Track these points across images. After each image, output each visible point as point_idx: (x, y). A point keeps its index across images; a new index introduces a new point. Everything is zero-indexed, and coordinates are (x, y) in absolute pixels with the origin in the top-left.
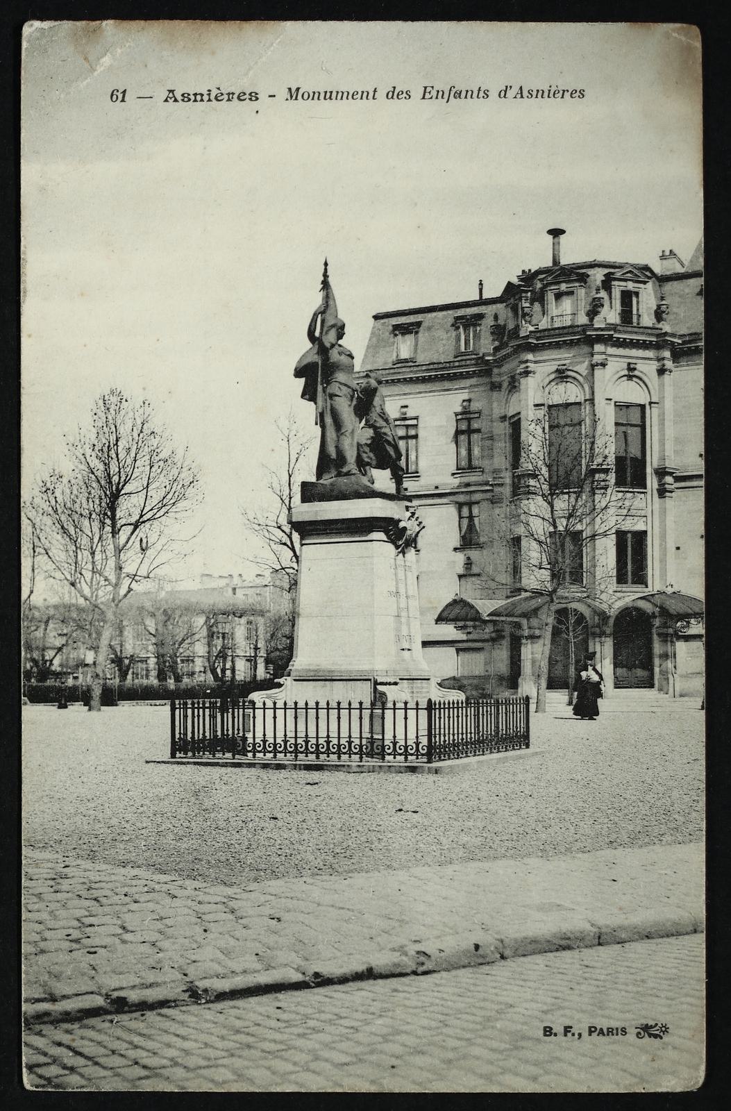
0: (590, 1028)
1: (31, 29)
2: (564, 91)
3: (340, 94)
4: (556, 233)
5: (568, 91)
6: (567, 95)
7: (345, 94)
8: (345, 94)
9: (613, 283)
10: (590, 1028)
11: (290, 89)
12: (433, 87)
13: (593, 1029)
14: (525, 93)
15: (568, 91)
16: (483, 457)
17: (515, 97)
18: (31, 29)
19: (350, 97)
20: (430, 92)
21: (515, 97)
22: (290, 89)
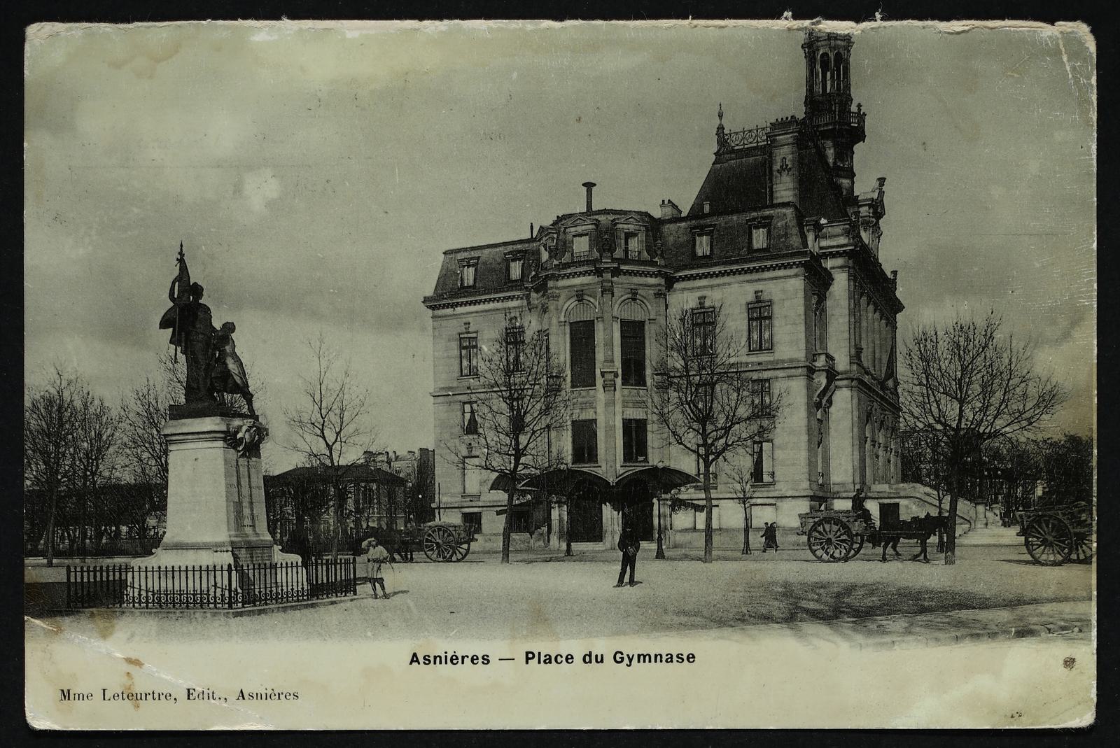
0: (527, 653)
1: (1084, 717)
2: (463, 657)
3: (77, 696)
4: (589, 186)
5: (468, 657)
6: (467, 661)
7: (81, 696)
8: (81, 696)
9: (336, 464)
10: (527, 653)
11: (63, 691)
12: (194, 690)
13: (530, 656)
14: (246, 696)
15: (468, 657)
16: (830, 111)
17: (238, 699)
18: (1084, 717)
19: (85, 697)
20: (192, 694)
21: (238, 699)
22: (63, 691)
